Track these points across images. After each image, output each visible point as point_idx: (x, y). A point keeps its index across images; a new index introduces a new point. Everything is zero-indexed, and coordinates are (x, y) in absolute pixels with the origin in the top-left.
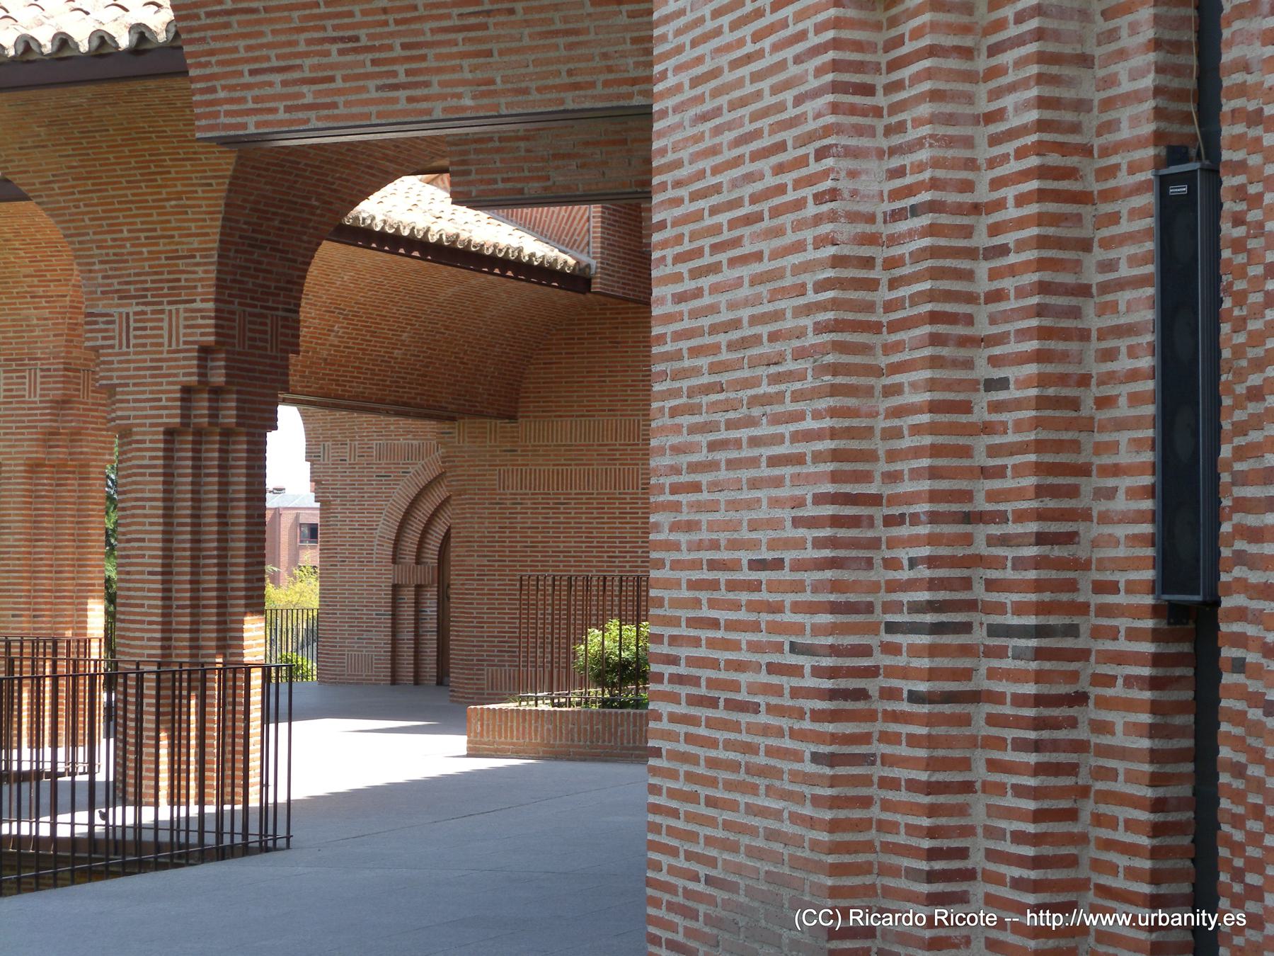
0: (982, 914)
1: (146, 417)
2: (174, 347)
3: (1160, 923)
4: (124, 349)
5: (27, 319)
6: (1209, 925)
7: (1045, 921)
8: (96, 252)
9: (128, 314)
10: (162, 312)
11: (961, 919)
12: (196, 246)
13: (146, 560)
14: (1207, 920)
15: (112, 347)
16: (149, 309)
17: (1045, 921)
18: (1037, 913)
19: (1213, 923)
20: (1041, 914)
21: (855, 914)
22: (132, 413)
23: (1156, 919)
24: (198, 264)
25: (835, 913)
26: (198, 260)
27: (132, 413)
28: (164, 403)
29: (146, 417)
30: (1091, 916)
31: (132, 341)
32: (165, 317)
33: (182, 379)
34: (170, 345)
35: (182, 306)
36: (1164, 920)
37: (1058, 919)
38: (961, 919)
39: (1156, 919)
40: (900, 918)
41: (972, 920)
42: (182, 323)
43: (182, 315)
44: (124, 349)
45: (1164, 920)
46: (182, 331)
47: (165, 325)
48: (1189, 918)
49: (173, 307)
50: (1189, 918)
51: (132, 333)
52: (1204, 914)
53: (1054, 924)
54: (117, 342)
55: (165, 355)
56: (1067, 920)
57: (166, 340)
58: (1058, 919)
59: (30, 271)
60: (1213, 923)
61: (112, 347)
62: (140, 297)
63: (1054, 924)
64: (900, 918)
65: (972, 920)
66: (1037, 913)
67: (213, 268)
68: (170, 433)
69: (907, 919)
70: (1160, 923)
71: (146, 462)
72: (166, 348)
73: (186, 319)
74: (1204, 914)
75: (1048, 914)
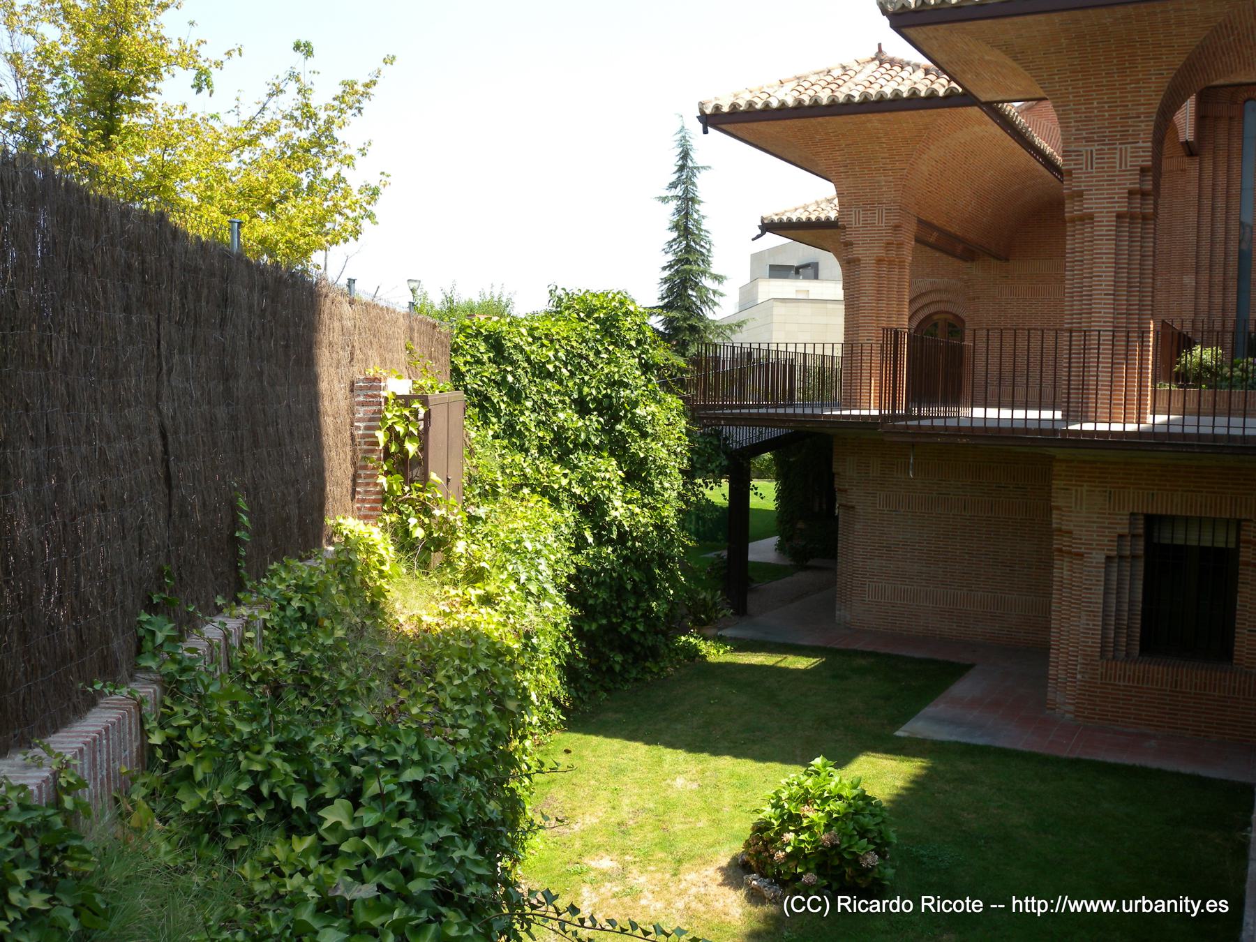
0: (968, 901)
1: (1104, 208)
2: (1123, 168)
3: (1144, 910)
4: (1089, 170)
5: (879, 182)
6: (1192, 912)
7: (1030, 908)
8: (1073, 115)
9: (1092, 151)
10: (1116, 149)
11: (947, 906)
12: (1142, 111)
13: (1103, 287)
14: (1190, 907)
15: (1081, 169)
16: (1106, 147)
17: (1030, 908)
18: (1023, 900)
19: (1196, 910)
20: (1027, 901)
21: (843, 901)
22: (1094, 206)
23: (1140, 905)
24: (1142, 122)
25: (823, 899)
26: (1142, 118)
27: (1094, 206)
28: (1116, 200)
29: (1104, 208)
30: (1076, 902)
31: (1095, 166)
32: (1118, 152)
33: (1128, 186)
34: (1121, 166)
35: (1129, 146)
36: (1147, 906)
37: (1043, 906)
38: (947, 906)
39: (1140, 905)
40: (887, 905)
41: (959, 906)
42: (1129, 155)
43: (1129, 150)
44: (1089, 170)
45: (1147, 906)
46: (1129, 159)
47: (1118, 156)
48: (1172, 905)
49: (1123, 146)
50: (1172, 905)
51: (1094, 161)
52: (1187, 901)
53: (1039, 910)
54: (1084, 166)
55: (1117, 173)
56: (1052, 906)
57: (1118, 165)
58: (1043, 906)
59: (887, 155)
60: (1196, 910)
61: (1081, 169)
62: (1101, 141)
63: (1039, 910)
64: (887, 905)
65: (959, 906)
66: (1023, 900)
67: (1152, 123)
68: (1119, 216)
69: (895, 906)
70: (1144, 910)
71: (1104, 233)
72: (1118, 168)
73: (1132, 152)
74: (1187, 901)
75: (1033, 901)
